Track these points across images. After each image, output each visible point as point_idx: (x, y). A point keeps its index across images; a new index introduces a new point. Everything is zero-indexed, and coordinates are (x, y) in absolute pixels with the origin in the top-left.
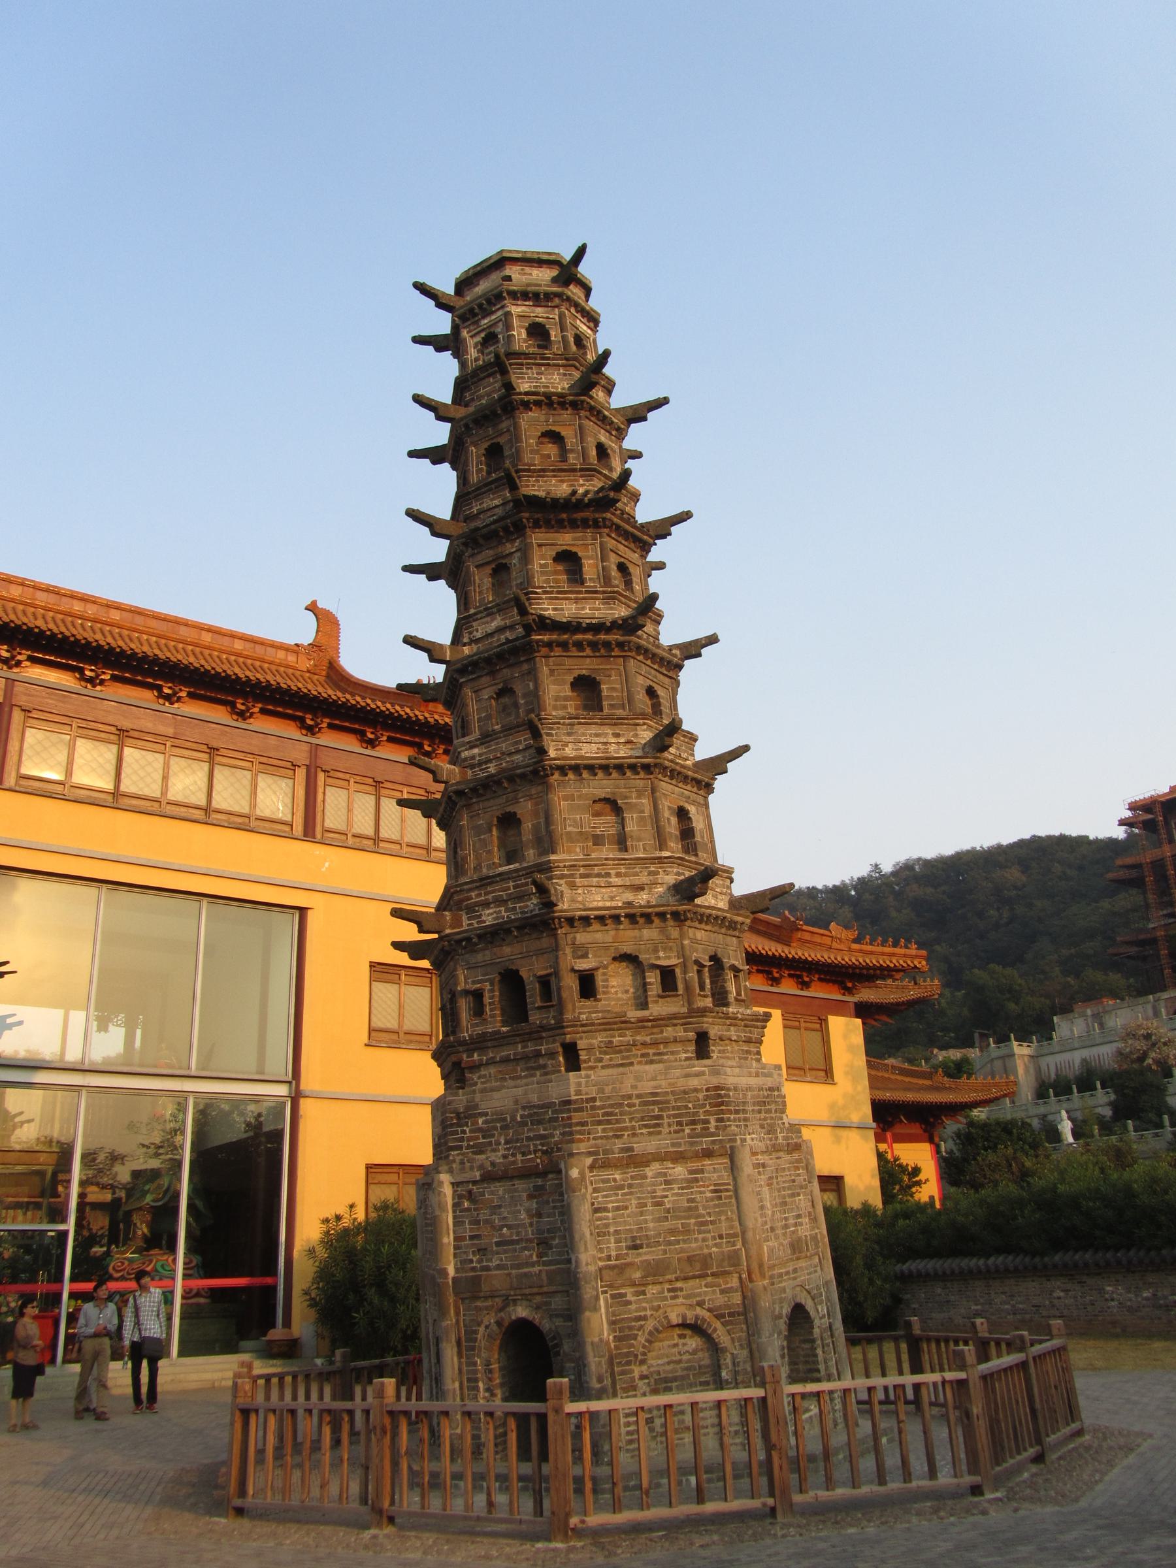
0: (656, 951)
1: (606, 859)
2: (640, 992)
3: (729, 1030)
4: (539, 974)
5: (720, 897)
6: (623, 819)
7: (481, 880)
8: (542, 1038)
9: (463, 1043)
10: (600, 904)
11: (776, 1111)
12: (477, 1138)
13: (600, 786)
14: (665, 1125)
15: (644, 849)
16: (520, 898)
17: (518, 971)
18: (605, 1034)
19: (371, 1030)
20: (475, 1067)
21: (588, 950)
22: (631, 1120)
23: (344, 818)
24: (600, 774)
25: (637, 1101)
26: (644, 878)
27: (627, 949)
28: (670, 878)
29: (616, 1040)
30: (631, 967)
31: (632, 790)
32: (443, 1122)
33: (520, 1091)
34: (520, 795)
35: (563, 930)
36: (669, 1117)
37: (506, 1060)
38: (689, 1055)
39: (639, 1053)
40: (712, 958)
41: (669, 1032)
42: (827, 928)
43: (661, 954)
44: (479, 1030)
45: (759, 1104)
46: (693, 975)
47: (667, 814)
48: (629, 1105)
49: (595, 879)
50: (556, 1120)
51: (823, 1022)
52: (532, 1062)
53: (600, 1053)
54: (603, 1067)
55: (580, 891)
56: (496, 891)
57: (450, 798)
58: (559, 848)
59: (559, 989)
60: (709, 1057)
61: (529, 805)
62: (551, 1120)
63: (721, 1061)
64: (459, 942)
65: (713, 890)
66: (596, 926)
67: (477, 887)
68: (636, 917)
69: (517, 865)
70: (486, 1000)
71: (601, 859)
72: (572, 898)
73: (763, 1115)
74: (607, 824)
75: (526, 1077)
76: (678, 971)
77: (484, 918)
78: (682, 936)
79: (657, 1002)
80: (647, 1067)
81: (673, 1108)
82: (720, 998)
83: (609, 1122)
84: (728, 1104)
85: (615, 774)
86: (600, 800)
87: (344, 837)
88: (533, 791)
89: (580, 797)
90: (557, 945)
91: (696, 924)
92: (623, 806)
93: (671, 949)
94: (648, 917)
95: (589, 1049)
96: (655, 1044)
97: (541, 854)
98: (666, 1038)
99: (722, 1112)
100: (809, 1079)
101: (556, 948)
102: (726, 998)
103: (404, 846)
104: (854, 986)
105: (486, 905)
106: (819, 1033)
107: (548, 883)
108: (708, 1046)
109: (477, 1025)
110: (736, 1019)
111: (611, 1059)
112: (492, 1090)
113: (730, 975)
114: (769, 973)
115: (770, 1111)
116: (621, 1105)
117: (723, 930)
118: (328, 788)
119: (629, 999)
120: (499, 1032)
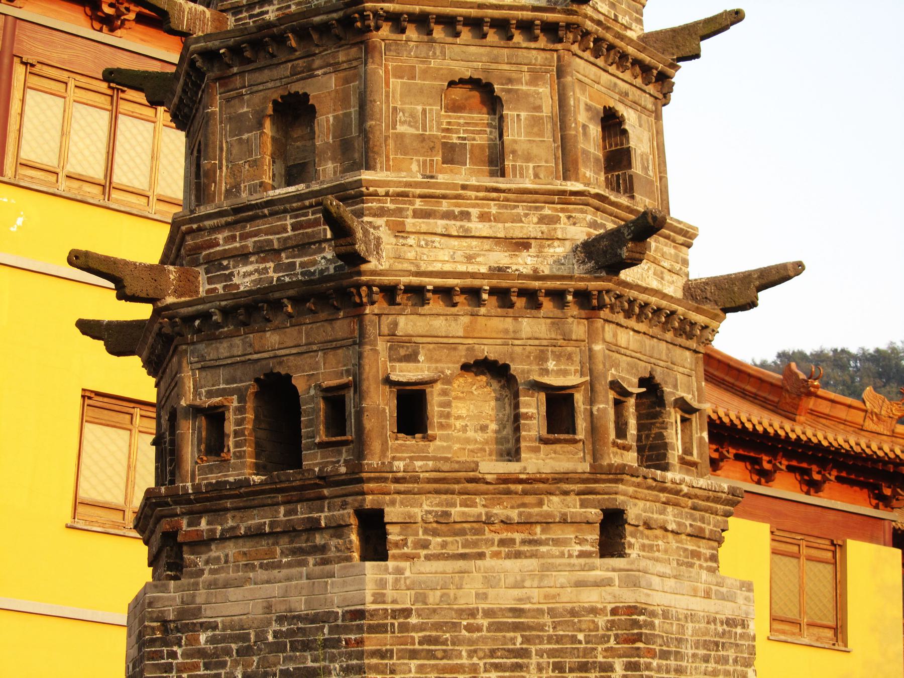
0: (542, 358)
1: (464, 187)
2: (508, 431)
3: (663, 512)
4: (326, 384)
5: (667, 276)
6: (501, 118)
7: (236, 210)
8: (324, 498)
9: (182, 499)
10: (448, 267)
11: (736, 661)
12: (196, 667)
13: (466, 56)
14: (533, 668)
15: (536, 176)
16: (303, 246)
17: (289, 377)
18: (437, 499)
19: (77, 503)
20: (202, 544)
21: (424, 345)
22: (471, 654)
23: (55, 145)
24: (466, 34)
25: (485, 622)
26: (530, 228)
27: (490, 351)
28: (579, 228)
29: (457, 511)
30: (496, 385)
31: (519, 67)
32: (140, 635)
33: (275, 589)
34: (318, 62)
35: (376, 309)
36: (540, 654)
37: (256, 534)
38: (587, 548)
39: (497, 537)
40: (642, 382)
41: (554, 505)
42: (857, 394)
43: (551, 365)
44: (213, 478)
45: (706, 645)
46: (605, 407)
47: (582, 117)
48: (470, 628)
49: (441, 222)
50: (336, 643)
51: (837, 547)
52: (303, 540)
53: (426, 531)
54: (428, 558)
55: (411, 240)
56: (265, 232)
57: (192, 63)
58: (380, 161)
59: (360, 413)
60: (622, 555)
61: (332, 82)
62: (327, 644)
63: (643, 564)
64: (188, 320)
65: (655, 261)
66: (436, 305)
67: (228, 225)
68: (507, 295)
69: (301, 188)
70: (230, 427)
71: (454, 186)
72: (395, 250)
73: (711, 666)
74: (472, 128)
75: (289, 565)
76: (579, 398)
77: (236, 280)
78: (592, 335)
79: (536, 450)
80: (509, 564)
81: (550, 639)
82: (653, 453)
83: (431, 655)
84: (649, 639)
85: (493, 37)
86: (462, 82)
87: (52, 178)
88: (342, 57)
89: (425, 73)
90: (362, 334)
91: (620, 318)
92: (504, 96)
93: (569, 357)
94: (532, 298)
95: (406, 524)
96: (527, 523)
97: (345, 171)
98: (549, 515)
99: (637, 652)
100: (806, 641)
101: (359, 340)
102: (664, 456)
103: (153, 200)
104: (895, 495)
105: (243, 256)
106: (830, 568)
107: (355, 224)
108: (623, 536)
109: (211, 470)
110: (678, 493)
111: (444, 545)
112: (226, 585)
113: (674, 416)
114: (755, 462)
115: (725, 660)
116: (455, 626)
117: (669, 336)
118: (30, 93)
119: (487, 442)
120: (246, 483)
